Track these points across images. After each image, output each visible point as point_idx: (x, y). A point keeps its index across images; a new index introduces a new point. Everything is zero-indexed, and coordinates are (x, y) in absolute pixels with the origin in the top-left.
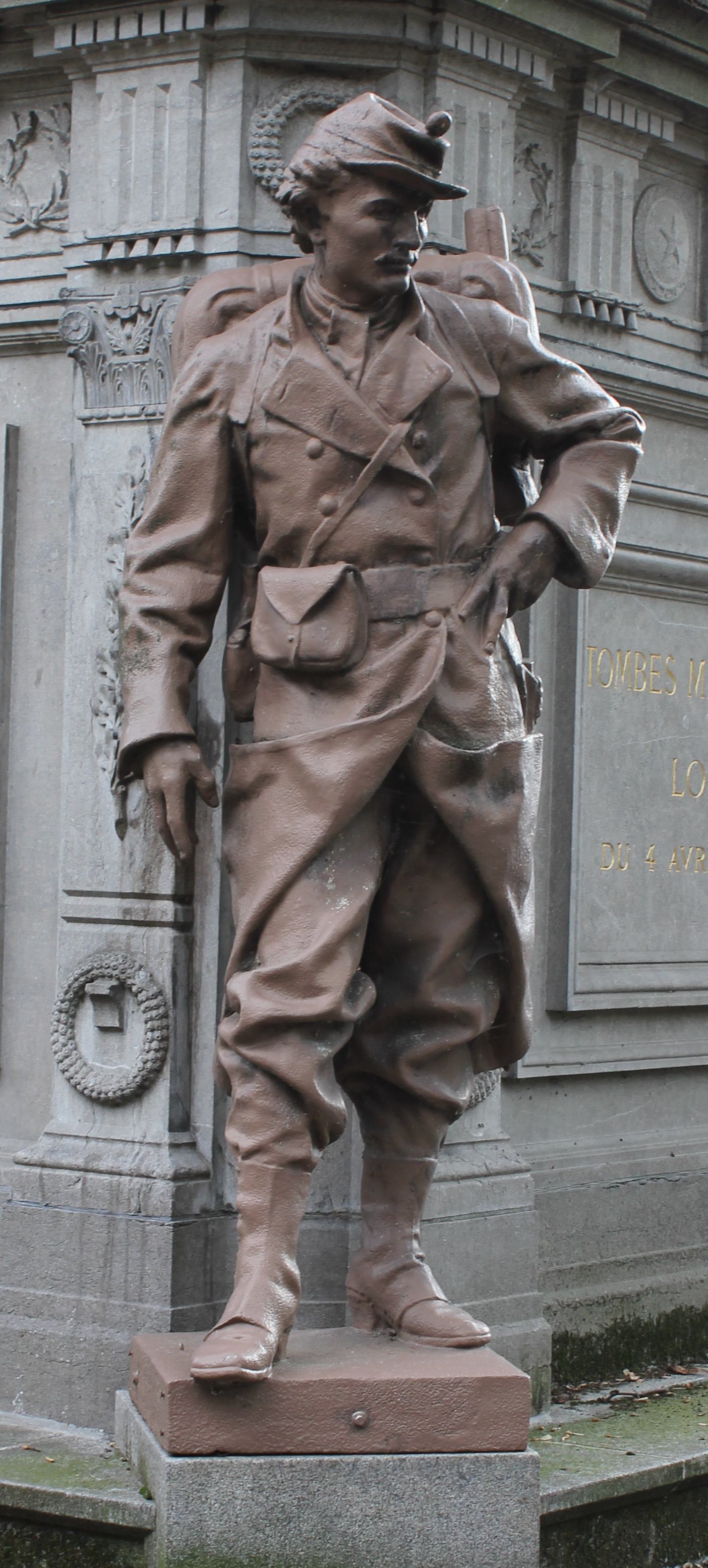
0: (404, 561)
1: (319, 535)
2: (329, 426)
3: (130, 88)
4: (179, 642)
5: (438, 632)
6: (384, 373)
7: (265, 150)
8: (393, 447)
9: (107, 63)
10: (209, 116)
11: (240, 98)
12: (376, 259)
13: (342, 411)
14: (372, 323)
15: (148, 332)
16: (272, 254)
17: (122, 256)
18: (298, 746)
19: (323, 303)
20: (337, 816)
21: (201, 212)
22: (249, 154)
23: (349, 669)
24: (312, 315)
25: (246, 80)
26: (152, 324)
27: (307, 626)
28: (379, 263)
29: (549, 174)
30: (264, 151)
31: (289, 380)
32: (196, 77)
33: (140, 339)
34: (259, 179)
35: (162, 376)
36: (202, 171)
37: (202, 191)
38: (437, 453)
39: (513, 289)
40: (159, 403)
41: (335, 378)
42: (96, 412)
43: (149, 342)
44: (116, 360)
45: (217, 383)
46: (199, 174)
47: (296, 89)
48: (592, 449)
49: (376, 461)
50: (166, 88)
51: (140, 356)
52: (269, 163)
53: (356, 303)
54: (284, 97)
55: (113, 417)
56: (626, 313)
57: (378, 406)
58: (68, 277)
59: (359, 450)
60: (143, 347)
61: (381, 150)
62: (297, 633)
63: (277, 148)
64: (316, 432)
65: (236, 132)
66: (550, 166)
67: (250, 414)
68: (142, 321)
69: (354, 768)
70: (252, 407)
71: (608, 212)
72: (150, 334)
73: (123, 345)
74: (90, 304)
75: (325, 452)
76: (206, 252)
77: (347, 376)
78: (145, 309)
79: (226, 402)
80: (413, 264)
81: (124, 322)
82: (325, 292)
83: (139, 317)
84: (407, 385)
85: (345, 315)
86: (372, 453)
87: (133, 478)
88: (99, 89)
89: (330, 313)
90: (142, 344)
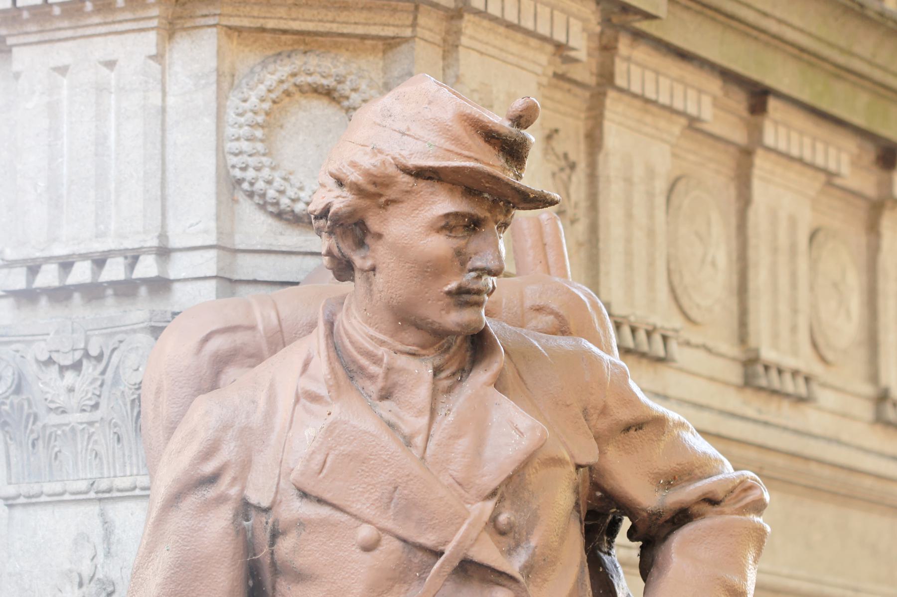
2: (388, 507)
3: (60, 64)
6: (458, 437)
7: (246, 143)
8: (474, 535)
9: (27, 33)
10: (171, 100)
11: (213, 78)
12: (446, 289)
13: (405, 488)
14: (437, 371)
15: (99, 383)
16: (258, 279)
17: (56, 283)
19: (369, 346)
21: (164, 225)
22: (226, 150)
24: (354, 362)
25: (220, 54)
26: (103, 373)
28: (449, 293)
29: (573, 166)
30: (245, 145)
31: (331, 448)
32: (153, 51)
33: (87, 393)
34: (239, 182)
35: (119, 440)
36: (164, 172)
37: (164, 198)
39: (591, 321)
40: (115, 476)
41: (389, 444)
42: (24, 489)
43: (99, 396)
44: (54, 419)
45: (228, 453)
46: (159, 175)
49: (452, 554)
50: (110, 64)
51: (87, 414)
52: (252, 161)
53: (413, 345)
54: (269, 76)
55: (49, 495)
56: (665, 338)
57: (451, 480)
59: (429, 539)
60: (92, 403)
61: (453, 148)
63: (262, 141)
65: (209, 122)
66: (572, 157)
67: (277, 493)
68: (88, 368)
70: (278, 484)
71: (640, 212)
72: (102, 385)
73: (62, 400)
74: (14, 346)
75: (383, 542)
76: (172, 277)
77: (408, 442)
78: (94, 352)
79: (241, 478)
80: (490, 294)
81: (63, 369)
82: (372, 332)
83: (85, 362)
84: (488, 452)
85: (403, 361)
86: (446, 543)
87: (80, 576)
88: (16, 66)
89: (381, 360)
90: (90, 399)
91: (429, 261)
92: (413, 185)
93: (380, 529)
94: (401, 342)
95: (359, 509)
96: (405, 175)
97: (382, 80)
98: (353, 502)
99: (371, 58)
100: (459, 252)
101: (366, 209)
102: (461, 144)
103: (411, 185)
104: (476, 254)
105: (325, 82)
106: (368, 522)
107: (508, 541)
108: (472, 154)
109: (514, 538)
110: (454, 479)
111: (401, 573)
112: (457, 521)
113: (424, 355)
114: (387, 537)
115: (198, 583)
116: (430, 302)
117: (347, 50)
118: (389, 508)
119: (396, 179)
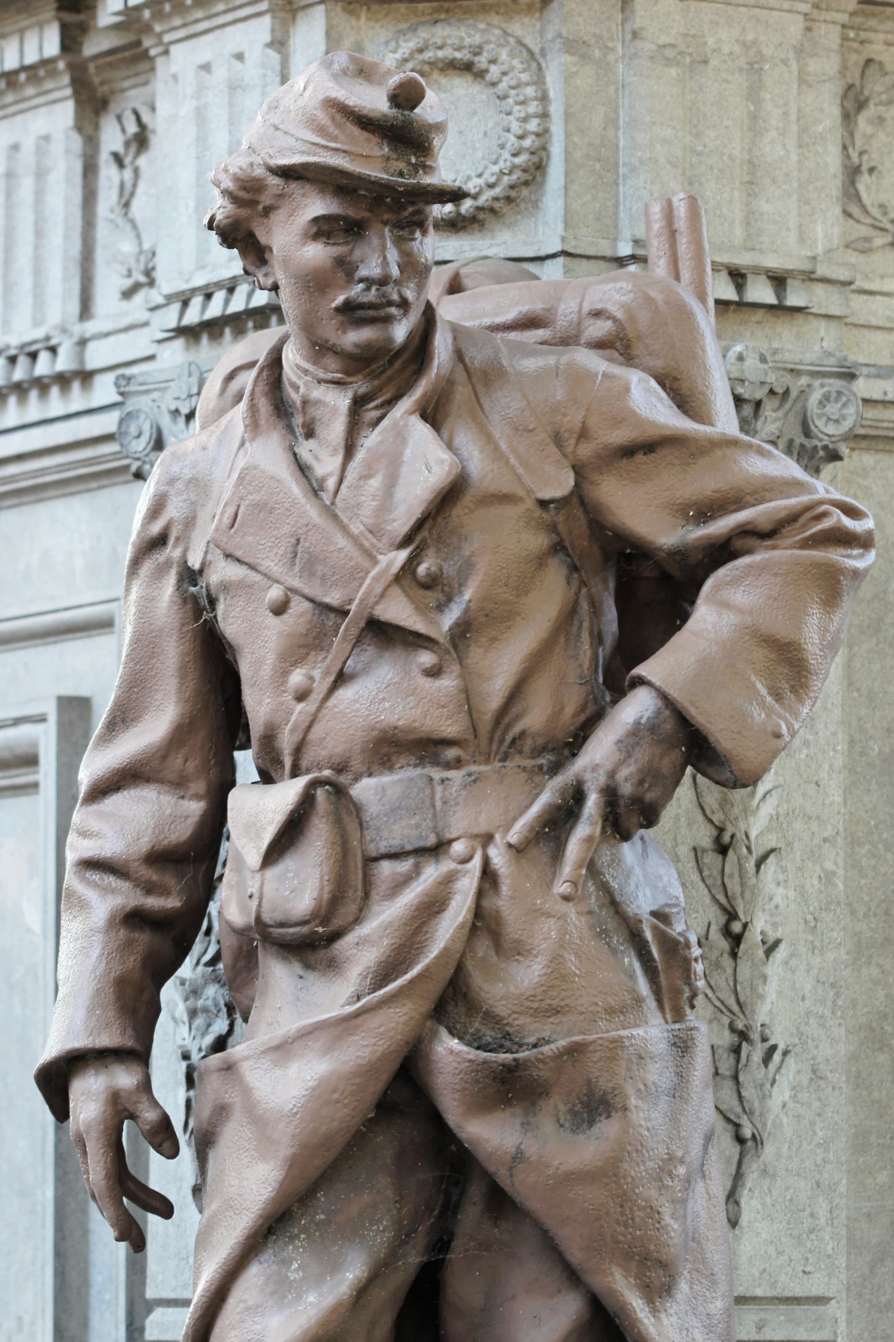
0: (421, 762)
1: (292, 731)
4: (123, 907)
5: (467, 872)
8: (379, 589)
12: (334, 305)
18: (246, 1058)
20: (294, 1164)
23: (336, 936)
27: (272, 873)
28: (337, 309)
31: (242, 499)
38: (461, 592)
47: (408, 40)
48: (750, 566)
49: (356, 613)
53: (337, 372)
54: (391, 55)
57: (362, 528)
58: (158, 356)
59: (333, 598)
62: (257, 885)
64: (277, 575)
69: (314, 1089)
75: (292, 604)
79: (184, 539)
86: (350, 601)
91: (307, 275)
92: (284, 188)
93: (291, 589)
94: (324, 369)
95: (268, 567)
96: (273, 177)
97: (540, 46)
98: (263, 559)
99: (526, 20)
100: (341, 261)
101: (249, 219)
102: (326, 134)
103: (281, 188)
104: (362, 262)
105: (458, 55)
106: (277, 581)
107: (432, 598)
108: (339, 146)
109: (443, 591)
110: (364, 525)
111: (315, 638)
112: (360, 575)
113: (351, 383)
114: (297, 597)
115: (155, 660)
116: (324, 322)
117: (498, 13)
118: (295, 564)
119: (267, 183)
